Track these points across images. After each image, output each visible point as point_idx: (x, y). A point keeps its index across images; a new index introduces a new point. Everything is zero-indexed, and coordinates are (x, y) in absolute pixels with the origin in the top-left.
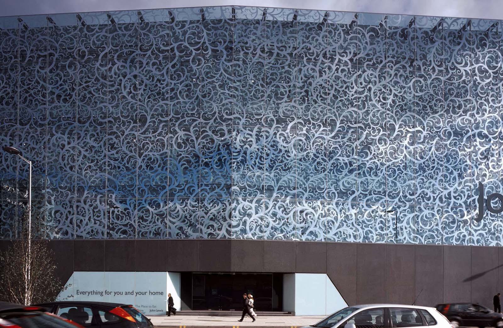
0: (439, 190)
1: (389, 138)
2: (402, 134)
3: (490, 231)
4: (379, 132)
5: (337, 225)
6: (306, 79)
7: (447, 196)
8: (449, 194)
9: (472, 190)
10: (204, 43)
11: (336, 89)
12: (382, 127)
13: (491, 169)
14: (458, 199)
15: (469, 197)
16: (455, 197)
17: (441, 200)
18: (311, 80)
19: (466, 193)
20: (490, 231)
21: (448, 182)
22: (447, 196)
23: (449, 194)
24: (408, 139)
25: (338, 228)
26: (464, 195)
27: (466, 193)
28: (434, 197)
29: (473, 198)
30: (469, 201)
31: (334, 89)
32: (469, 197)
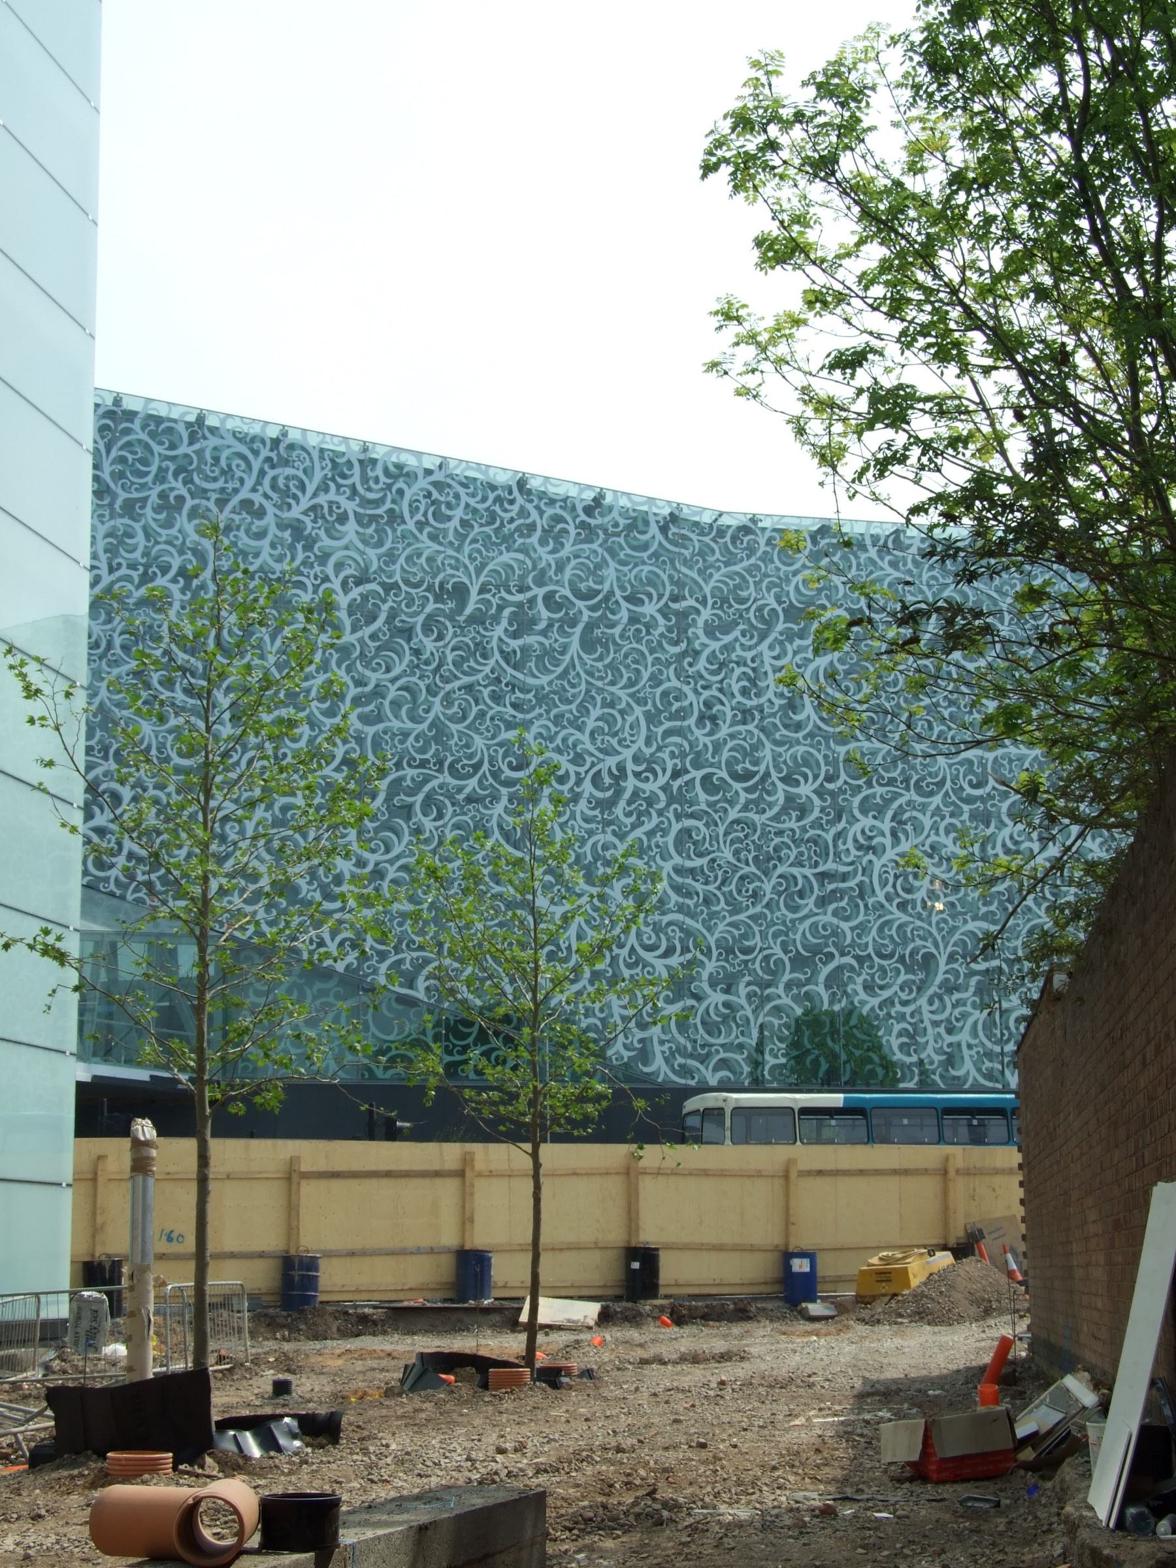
0: (592, 755)
1: (452, 620)
2: (561, 627)
3: (308, 548)
4: (423, 606)
5: (310, 489)
6: (389, 481)
7: (615, 772)
8: (621, 768)
9: (686, 756)
10: (767, 774)
11: (467, 505)
12: (615, 643)
13: (137, 526)
14: (647, 779)
15: (676, 774)
16: (637, 775)
17: (596, 780)
18: (400, 484)
19: (669, 765)
20: (308, 548)
21: (616, 734)
22: (615, 772)
23: (621, 768)
24: (504, 623)
25: (315, 495)
26: (664, 770)
27: (669, 765)
28: (578, 774)
29: (687, 777)
30: (676, 784)
31: (463, 505)
32: (676, 774)
